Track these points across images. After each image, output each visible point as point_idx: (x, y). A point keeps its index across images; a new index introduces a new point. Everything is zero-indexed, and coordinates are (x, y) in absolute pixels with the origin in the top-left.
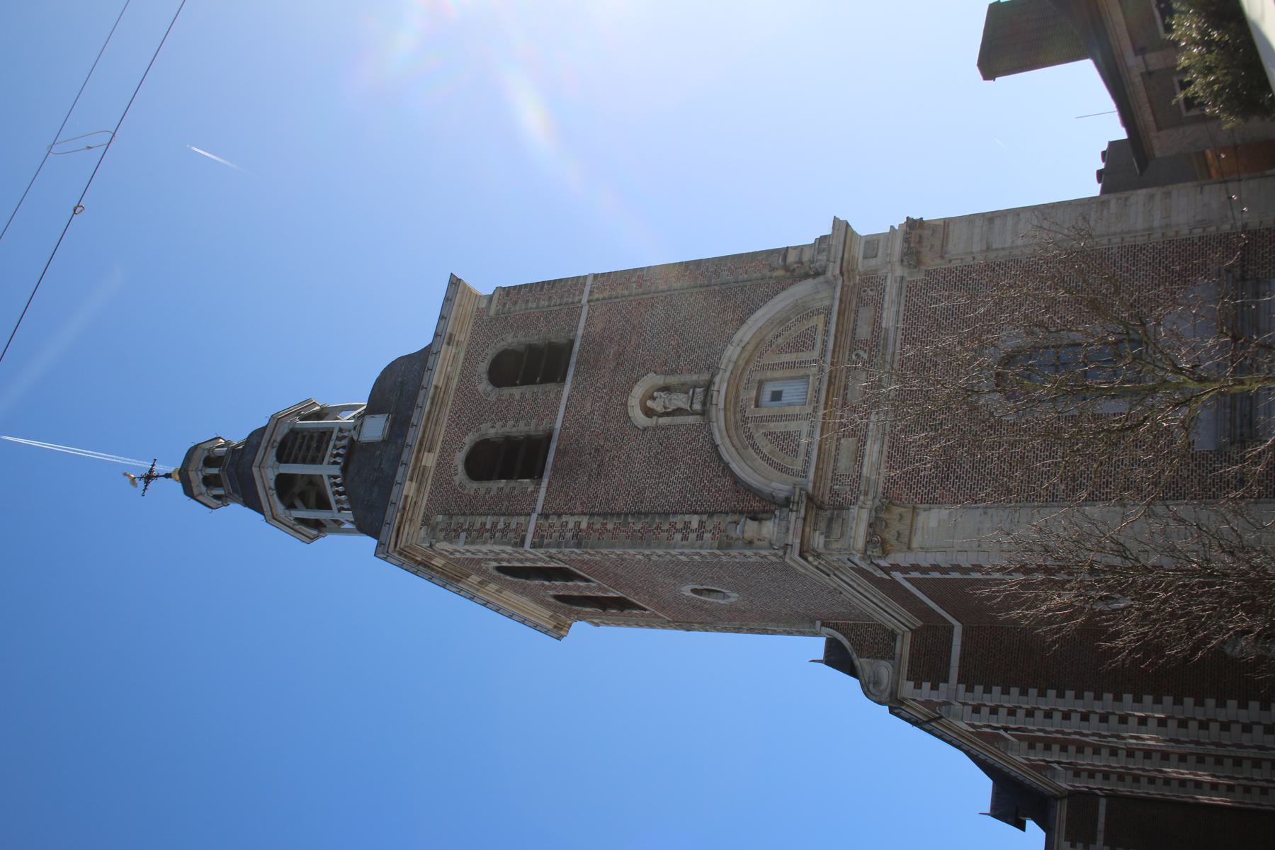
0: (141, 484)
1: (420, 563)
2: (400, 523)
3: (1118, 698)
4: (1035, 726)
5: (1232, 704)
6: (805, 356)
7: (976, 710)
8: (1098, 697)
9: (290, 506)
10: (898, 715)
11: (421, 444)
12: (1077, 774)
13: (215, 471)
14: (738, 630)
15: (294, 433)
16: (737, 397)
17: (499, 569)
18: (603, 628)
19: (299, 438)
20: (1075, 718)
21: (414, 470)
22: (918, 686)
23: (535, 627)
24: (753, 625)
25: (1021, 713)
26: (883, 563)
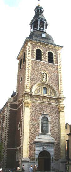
3: (8, 128)
4: (5, 118)
5: (7, 140)
6: (49, 93)
7: (7, 111)
8: (8, 125)
9: (34, 22)
12: (3, 117)
13: (39, 11)
14: (17, 82)
15: (44, 23)
17: (25, 53)
19: (43, 23)
20: (5, 131)
22: (10, 105)
23: (18, 56)
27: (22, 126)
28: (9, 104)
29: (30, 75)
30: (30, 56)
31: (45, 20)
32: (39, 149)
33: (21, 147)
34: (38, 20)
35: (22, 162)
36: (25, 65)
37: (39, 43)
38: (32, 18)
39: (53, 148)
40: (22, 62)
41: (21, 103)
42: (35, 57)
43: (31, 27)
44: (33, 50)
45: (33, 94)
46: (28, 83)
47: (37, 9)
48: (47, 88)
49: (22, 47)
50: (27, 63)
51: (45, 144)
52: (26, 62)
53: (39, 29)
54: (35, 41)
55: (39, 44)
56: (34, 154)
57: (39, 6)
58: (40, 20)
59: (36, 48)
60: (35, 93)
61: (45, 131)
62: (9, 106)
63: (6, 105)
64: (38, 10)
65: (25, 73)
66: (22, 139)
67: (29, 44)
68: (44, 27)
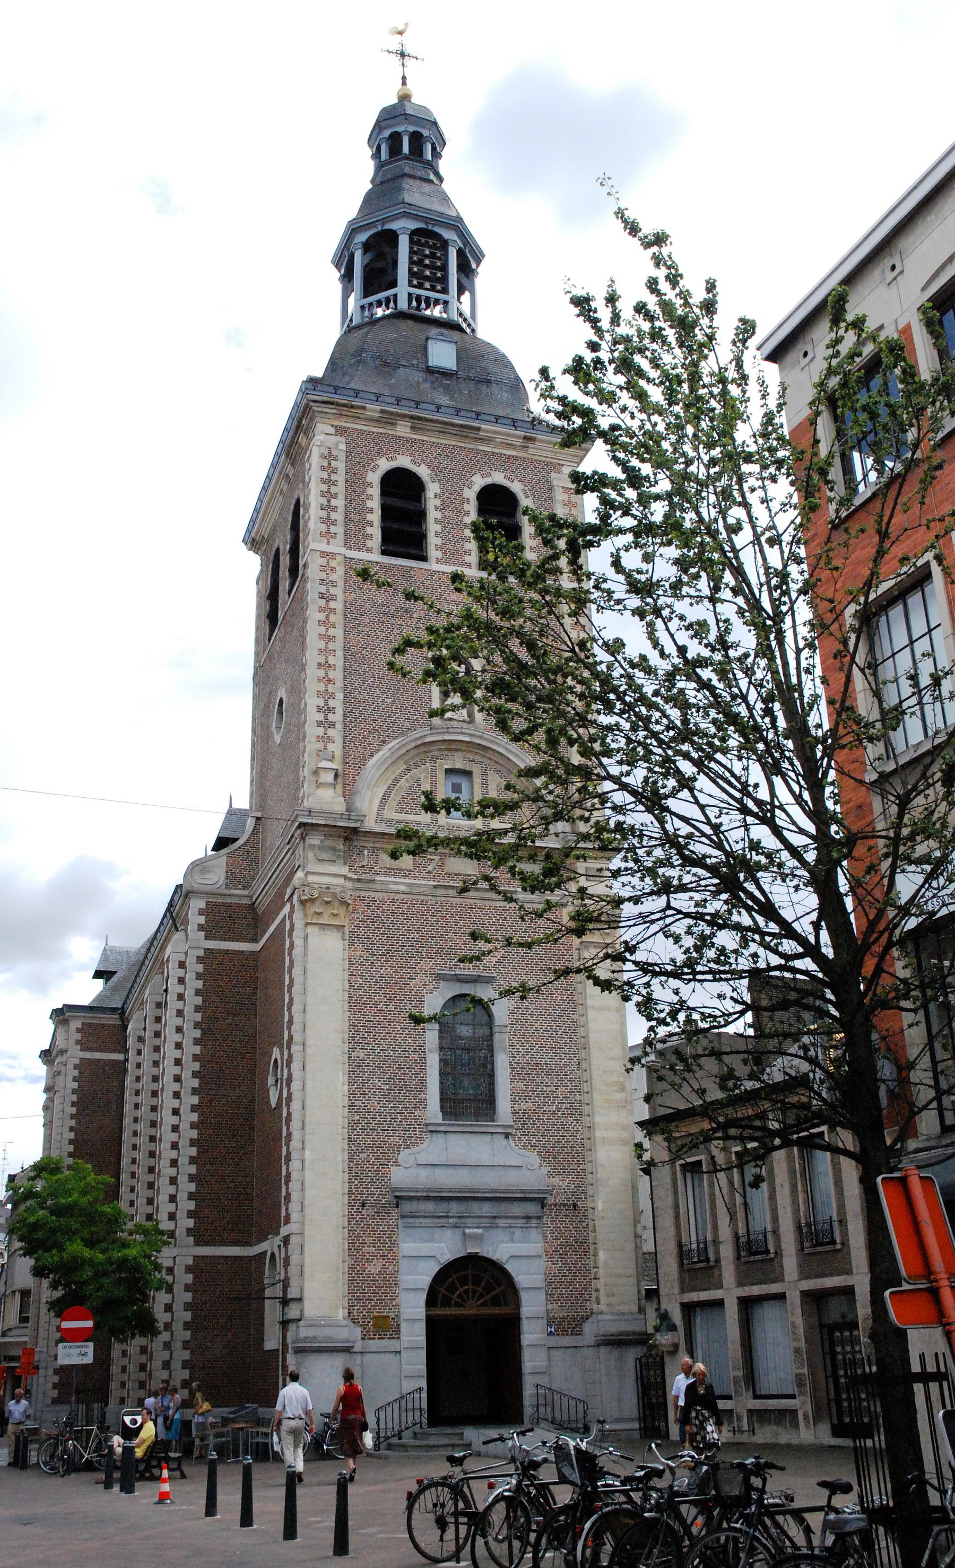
0: (396, 47)
1: (300, 422)
2: (338, 404)
4: (171, 1020)
9: (367, 247)
10: (175, 892)
11: (420, 419)
13: (406, 149)
14: (254, 731)
15: (444, 245)
16: (457, 750)
18: (35, 1097)
21: (391, 413)
22: (201, 912)
24: (258, 748)
25: (179, 1005)
26: (295, 898)
27: (290, 1080)
28: (197, 904)
29: (339, 684)
30: (339, 530)
31: (457, 225)
32: (424, 1248)
33: (286, 1240)
34: (394, 226)
35: (298, 1351)
36: (300, 604)
37: (404, 416)
38: (352, 209)
39: (535, 1234)
40: (284, 572)
41: (278, 902)
42: (375, 532)
43: (347, 277)
44: (355, 483)
45: (370, 824)
46: (321, 747)
47: (386, 133)
48: (476, 770)
49: (277, 454)
50: (313, 589)
51: (476, 1208)
52: (305, 580)
53: (403, 304)
54: (373, 409)
55: (403, 429)
56: (387, 1285)
57: (404, 98)
58: (414, 225)
59: (385, 465)
60: (379, 819)
61: (469, 1099)
62: (196, 919)
63: (174, 916)
64: (395, 139)
65: (303, 667)
66: (294, 1176)
67: (324, 436)
68: (444, 280)
